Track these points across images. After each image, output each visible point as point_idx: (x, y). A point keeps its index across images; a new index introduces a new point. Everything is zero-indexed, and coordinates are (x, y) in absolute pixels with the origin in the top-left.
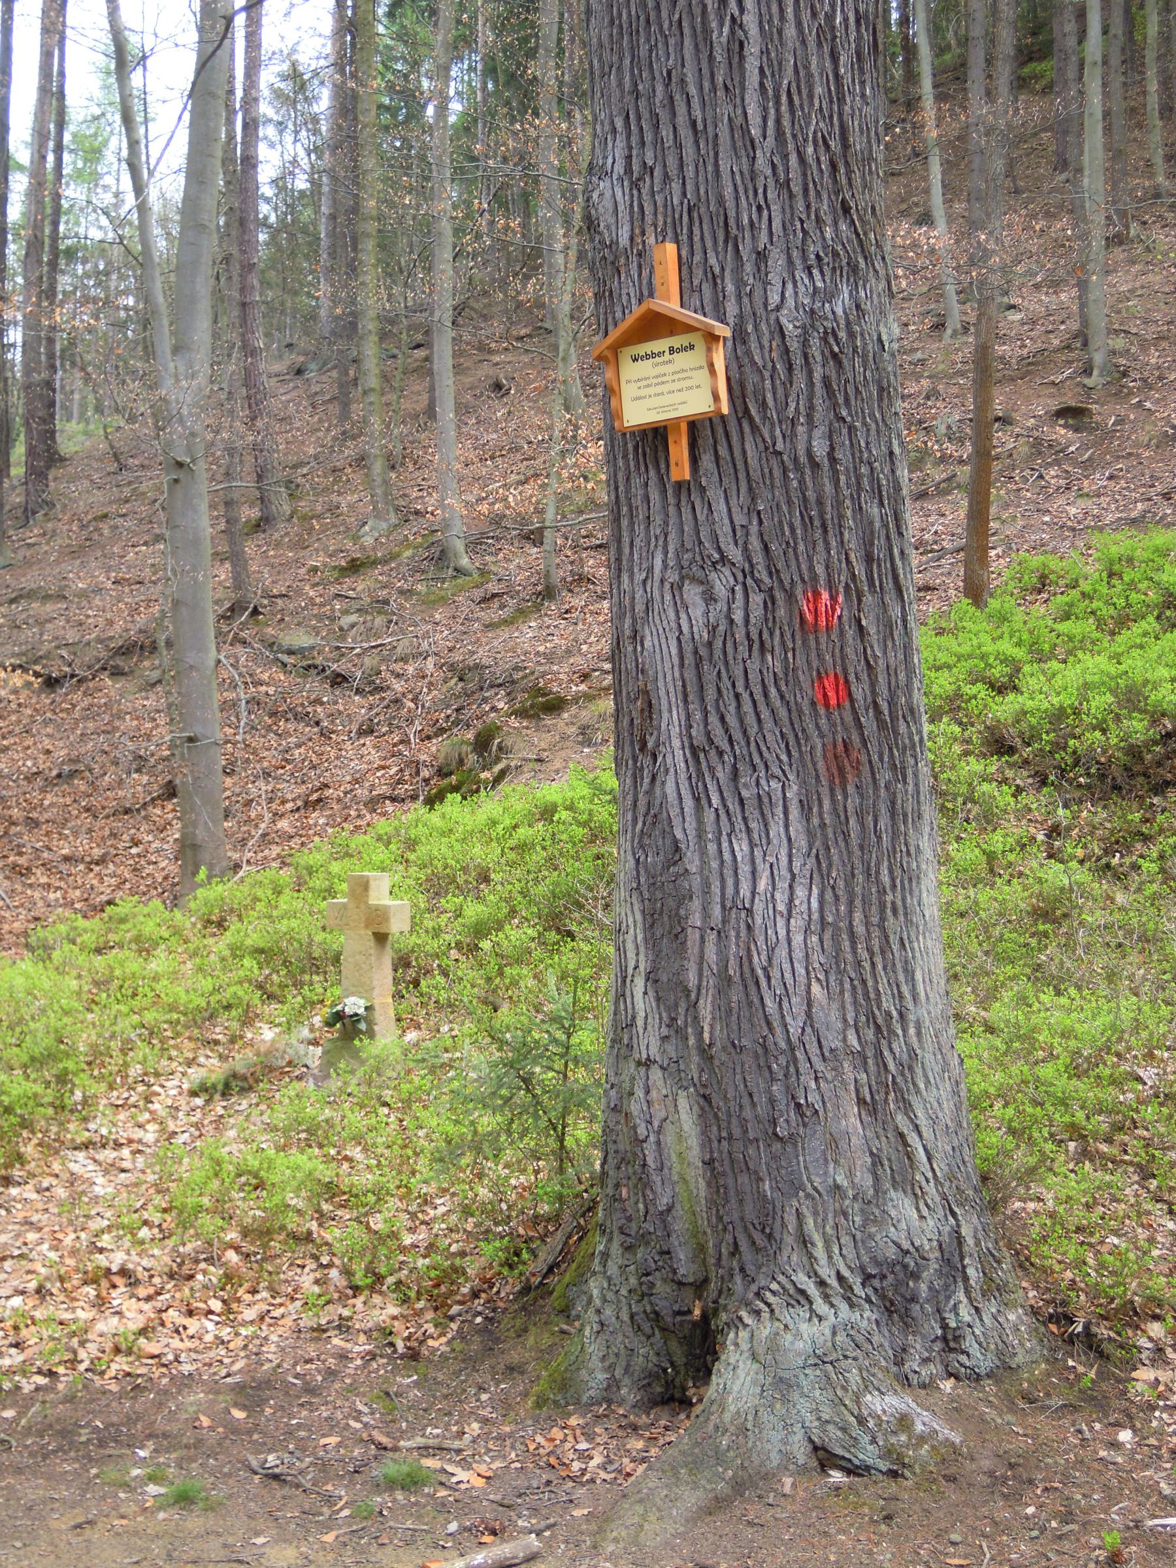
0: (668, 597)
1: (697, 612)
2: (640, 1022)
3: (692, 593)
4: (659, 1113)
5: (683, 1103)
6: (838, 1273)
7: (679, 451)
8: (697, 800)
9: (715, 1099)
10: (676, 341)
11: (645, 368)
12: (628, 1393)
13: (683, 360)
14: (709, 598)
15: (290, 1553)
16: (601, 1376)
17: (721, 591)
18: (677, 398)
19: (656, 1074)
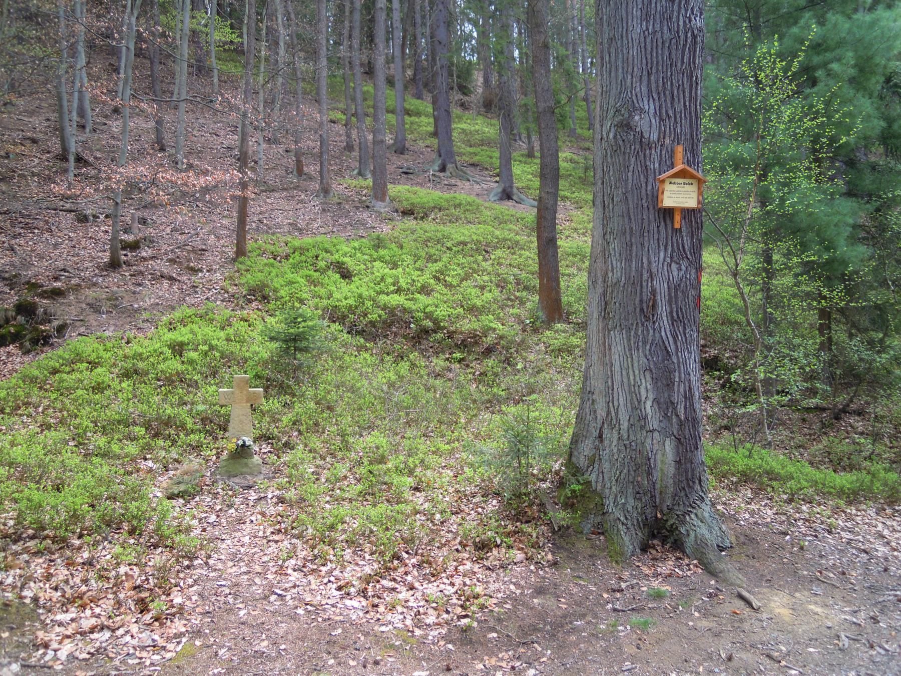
0: (665, 268)
1: (675, 274)
2: (649, 417)
3: (674, 266)
4: (656, 447)
5: (667, 443)
6: (841, 493)
7: (677, 218)
8: (674, 338)
9: (683, 440)
10: (687, 181)
11: (674, 187)
12: (638, 550)
13: (688, 188)
14: (680, 269)
15: (83, 674)
16: (631, 547)
17: (683, 268)
18: (684, 200)
19: (656, 434)
